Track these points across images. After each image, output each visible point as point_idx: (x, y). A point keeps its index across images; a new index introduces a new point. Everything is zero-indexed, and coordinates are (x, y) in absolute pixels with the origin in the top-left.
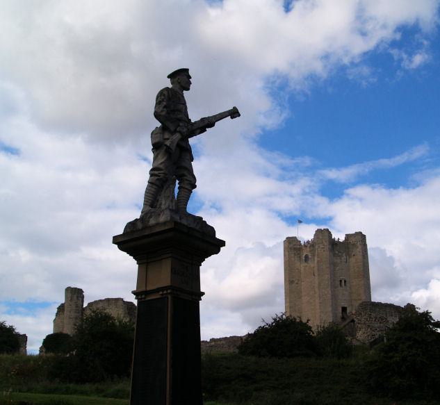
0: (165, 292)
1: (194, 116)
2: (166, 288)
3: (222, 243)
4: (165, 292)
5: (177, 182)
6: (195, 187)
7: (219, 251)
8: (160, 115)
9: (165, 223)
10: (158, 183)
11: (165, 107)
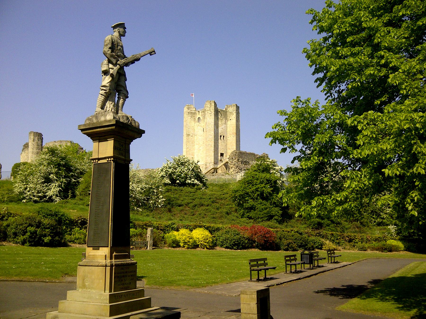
0: (110, 159)
1: (129, 54)
2: (110, 157)
3: (143, 132)
4: (110, 159)
5: (117, 93)
6: (128, 97)
7: (141, 136)
8: (107, 53)
9: (110, 121)
10: (105, 94)
11: (110, 48)
